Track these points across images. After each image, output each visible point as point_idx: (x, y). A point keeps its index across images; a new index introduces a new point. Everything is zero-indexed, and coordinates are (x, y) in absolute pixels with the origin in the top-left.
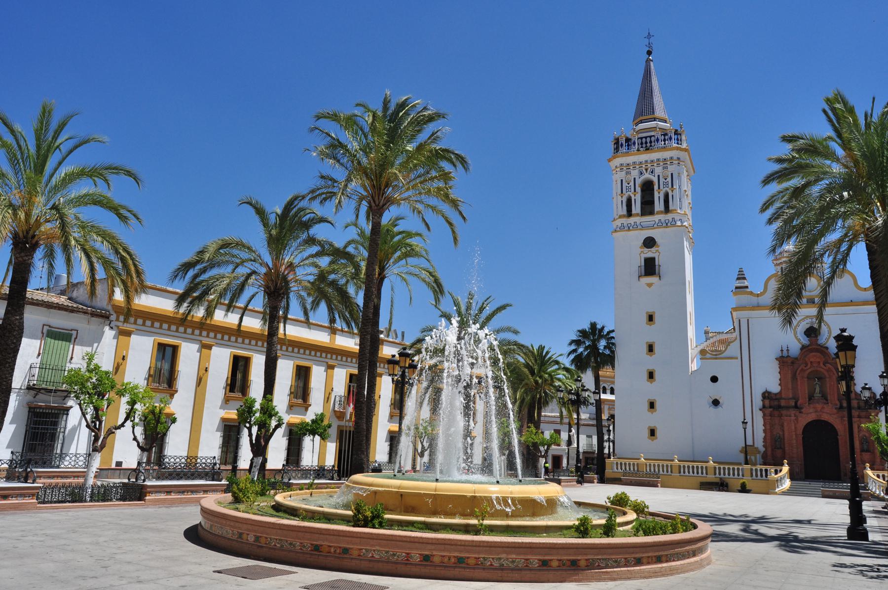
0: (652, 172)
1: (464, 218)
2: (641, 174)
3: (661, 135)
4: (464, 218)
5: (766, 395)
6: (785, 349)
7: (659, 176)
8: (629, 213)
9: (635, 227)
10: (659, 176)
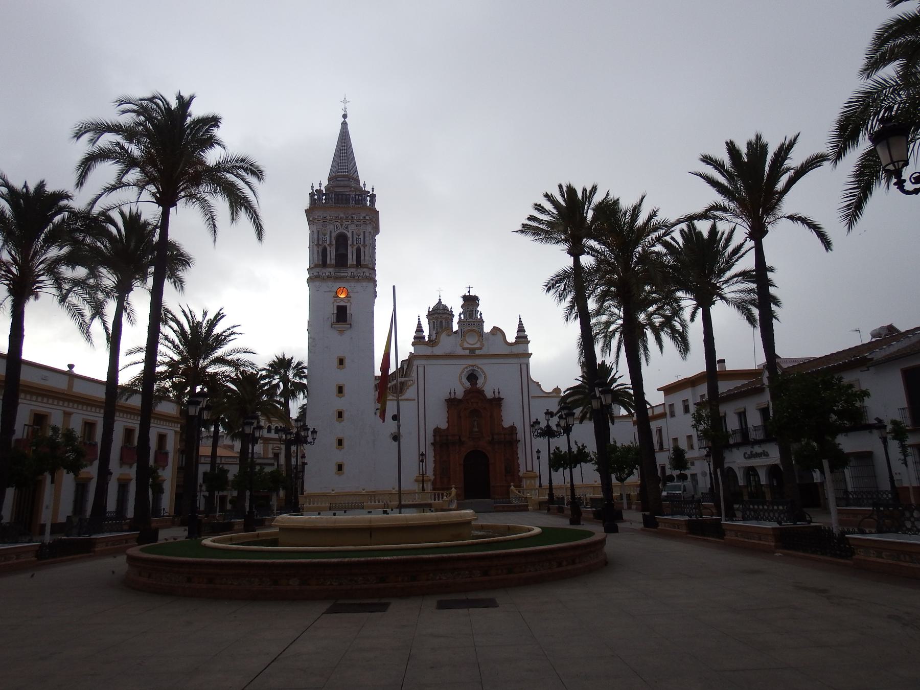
0: (347, 228)
2: (337, 228)
6: (452, 392)
7: (353, 232)
10: (353, 232)
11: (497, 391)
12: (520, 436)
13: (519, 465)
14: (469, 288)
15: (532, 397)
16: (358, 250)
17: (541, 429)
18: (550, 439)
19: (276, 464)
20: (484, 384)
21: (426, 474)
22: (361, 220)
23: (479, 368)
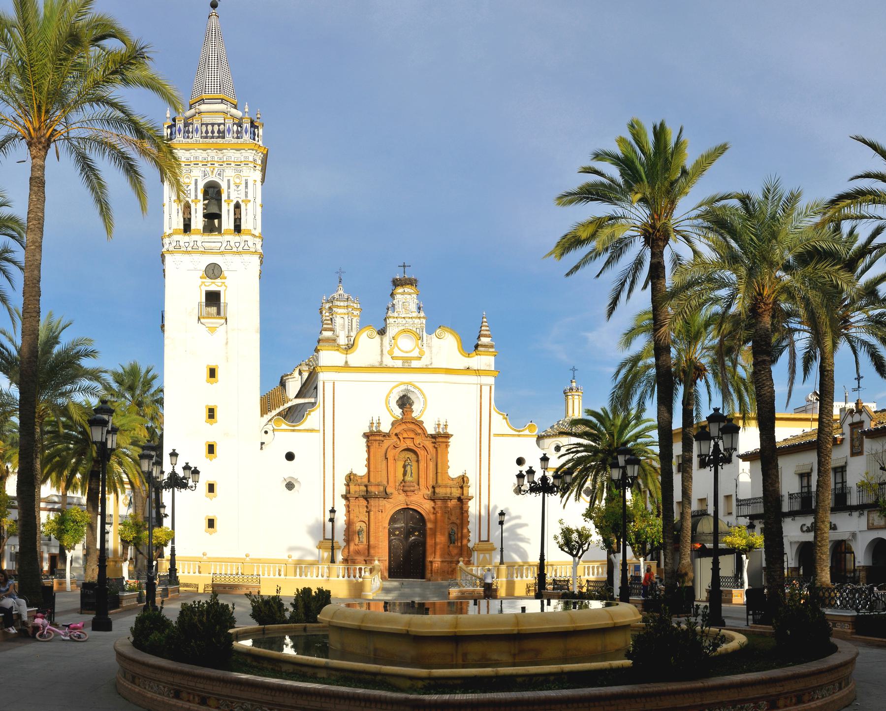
3: (234, 124)
5: (350, 478)
6: (442, 423)
7: (229, 181)
8: (187, 228)
9: (193, 250)
10: (229, 181)
12: (472, 491)
14: (404, 266)
16: (237, 206)
18: (546, 495)
20: (422, 412)
22: (191, 162)
23: (415, 387)
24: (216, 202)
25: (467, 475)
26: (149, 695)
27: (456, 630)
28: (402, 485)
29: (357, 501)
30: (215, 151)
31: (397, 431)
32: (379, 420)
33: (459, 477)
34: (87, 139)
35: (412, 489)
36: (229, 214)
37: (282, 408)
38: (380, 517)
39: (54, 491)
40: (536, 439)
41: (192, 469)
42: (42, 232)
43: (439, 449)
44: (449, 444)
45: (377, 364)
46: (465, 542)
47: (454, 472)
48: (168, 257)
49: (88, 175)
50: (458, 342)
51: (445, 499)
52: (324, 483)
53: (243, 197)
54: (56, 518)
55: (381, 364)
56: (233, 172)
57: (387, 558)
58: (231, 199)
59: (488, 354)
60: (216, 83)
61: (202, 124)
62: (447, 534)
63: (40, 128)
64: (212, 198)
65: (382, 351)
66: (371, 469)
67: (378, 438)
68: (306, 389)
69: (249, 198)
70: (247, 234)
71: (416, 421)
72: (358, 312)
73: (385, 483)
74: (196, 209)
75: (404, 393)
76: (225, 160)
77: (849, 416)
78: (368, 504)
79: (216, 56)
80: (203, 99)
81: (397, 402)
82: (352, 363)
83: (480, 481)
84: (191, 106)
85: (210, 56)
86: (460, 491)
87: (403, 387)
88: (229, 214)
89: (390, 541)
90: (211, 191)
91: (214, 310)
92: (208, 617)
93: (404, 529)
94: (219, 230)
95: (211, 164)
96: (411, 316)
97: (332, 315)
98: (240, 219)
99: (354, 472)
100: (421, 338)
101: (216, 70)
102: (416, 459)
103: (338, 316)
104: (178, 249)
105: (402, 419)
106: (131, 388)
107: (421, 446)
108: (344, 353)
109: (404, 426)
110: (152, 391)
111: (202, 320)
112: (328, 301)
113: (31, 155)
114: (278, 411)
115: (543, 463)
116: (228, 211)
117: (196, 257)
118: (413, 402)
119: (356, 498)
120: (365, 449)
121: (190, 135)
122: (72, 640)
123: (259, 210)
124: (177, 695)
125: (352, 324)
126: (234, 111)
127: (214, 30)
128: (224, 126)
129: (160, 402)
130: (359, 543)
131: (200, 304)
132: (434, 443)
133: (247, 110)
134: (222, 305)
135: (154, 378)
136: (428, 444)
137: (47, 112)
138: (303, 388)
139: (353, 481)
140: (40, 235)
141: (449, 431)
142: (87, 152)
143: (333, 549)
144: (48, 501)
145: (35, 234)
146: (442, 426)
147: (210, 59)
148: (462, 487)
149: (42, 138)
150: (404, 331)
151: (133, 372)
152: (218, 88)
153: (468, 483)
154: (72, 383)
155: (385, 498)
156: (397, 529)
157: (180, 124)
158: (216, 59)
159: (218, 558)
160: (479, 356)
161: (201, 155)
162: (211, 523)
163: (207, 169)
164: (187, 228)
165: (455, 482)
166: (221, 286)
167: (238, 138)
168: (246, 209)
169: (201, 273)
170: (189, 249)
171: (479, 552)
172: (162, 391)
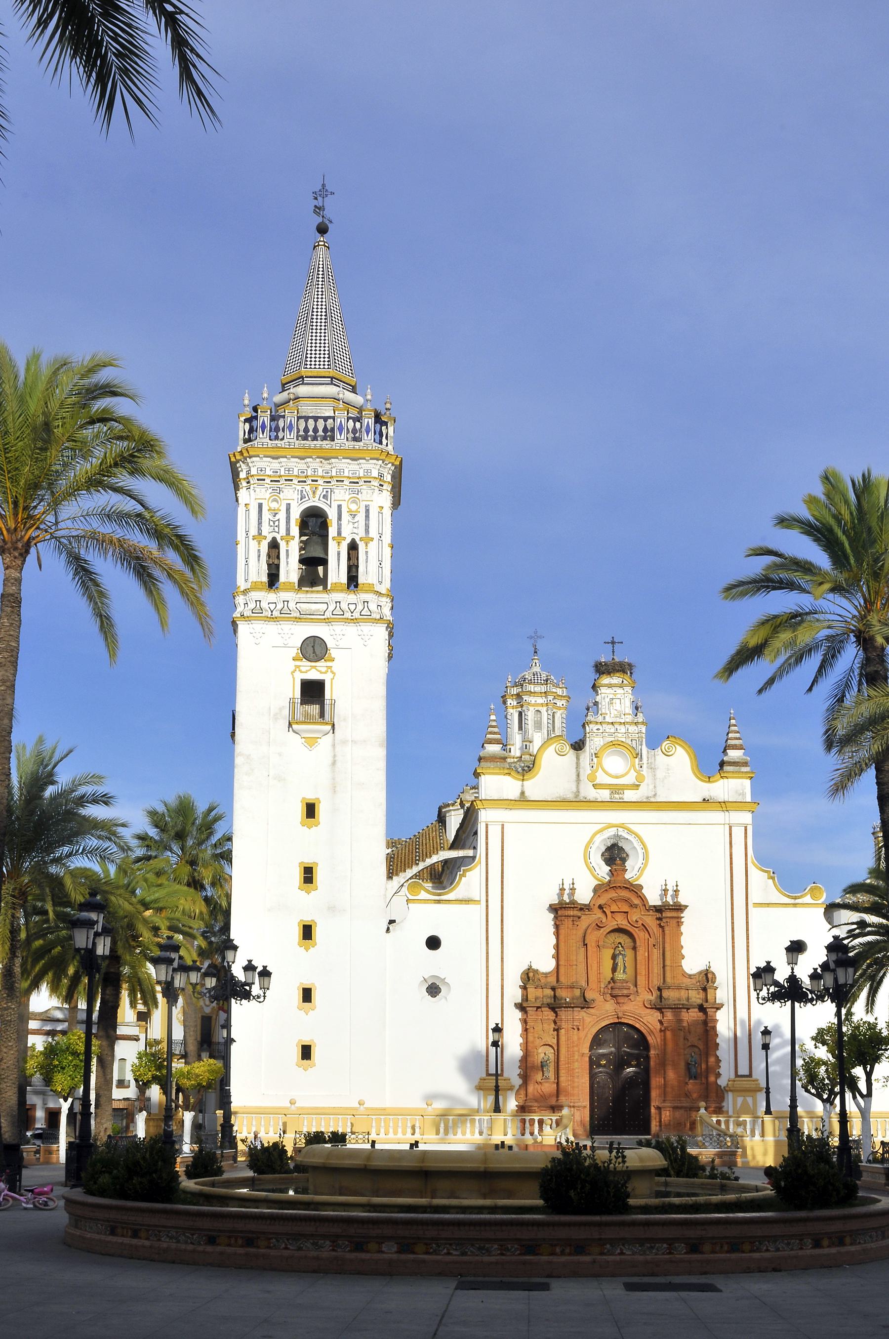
1: (810, 689)
3: (349, 418)
4: (810, 689)
5: (529, 977)
6: (670, 888)
7: (340, 507)
8: (273, 579)
10: (340, 507)
11: (670, 888)
12: (722, 994)
13: (718, 1061)
14: (613, 643)
15: (757, 905)
16: (353, 547)
17: (776, 983)
19: (142, 1037)
20: (641, 870)
21: (502, 1075)
22: (280, 476)
23: (630, 832)
24: (319, 540)
25: (711, 969)
26: (89, 1235)
27: (422, 1165)
28: (609, 987)
29: (539, 1013)
30: (318, 460)
31: (601, 901)
32: (573, 884)
33: (700, 973)
34: (81, 537)
35: (625, 992)
36: (339, 560)
37: (422, 865)
38: (575, 1038)
39: (55, 1002)
40: (823, 910)
41: (258, 970)
42: (16, 667)
43: (666, 929)
44: (683, 920)
45: (570, 796)
46: (712, 1079)
47: (692, 965)
48: (242, 627)
49: (84, 581)
50: (691, 759)
51: (677, 1009)
52: (487, 985)
53: (362, 533)
54: (45, 1048)
55: (577, 796)
56: (347, 492)
57: (587, 1103)
58: (342, 535)
59: (739, 775)
60: (322, 352)
61: (299, 418)
62: (682, 1065)
63: (16, 529)
64: (314, 533)
65: (578, 775)
66: (562, 963)
67: (571, 913)
68: (464, 832)
69: (371, 535)
70: (367, 591)
71: (632, 885)
72: (564, 702)
73: (583, 983)
74: (287, 551)
75: (612, 842)
76: (334, 474)
77: (221, 1012)
78: (556, 1017)
79: (324, 310)
80: (302, 377)
81: (602, 855)
82: (531, 795)
83: (734, 978)
84: (283, 385)
85: (315, 310)
86: (702, 995)
87: (612, 832)
88: (339, 560)
89: (592, 1076)
90: (312, 522)
91: (314, 709)
92: (151, 1154)
93: (615, 1057)
94: (324, 582)
95: (313, 481)
96: (622, 721)
97: (522, 706)
98: (357, 567)
99: (534, 967)
100: (638, 755)
101: (323, 331)
102: (632, 944)
103: (531, 708)
104: (258, 614)
105: (610, 881)
106: (180, 836)
107: (639, 924)
108: (518, 779)
109: (613, 894)
110: (214, 839)
111: (295, 726)
112: (516, 685)
113: (4, 564)
114: (415, 870)
115: (790, 955)
116: (339, 554)
117: (287, 627)
118: (627, 855)
119: (538, 1008)
120: (553, 930)
121: (281, 435)
122: (36, 1208)
123: (387, 552)
124: (113, 1232)
125: (554, 721)
126: (350, 396)
127: (321, 269)
128: (334, 421)
129: (227, 857)
130: (543, 1085)
131: (292, 701)
132: (659, 919)
133: (369, 397)
134: (327, 702)
135: (217, 819)
136: (650, 921)
137: (26, 508)
138: (461, 832)
139: (533, 981)
140: (12, 672)
141: (682, 900)
142: (82, 552)
143: (497, 1089)
144: (46, 1018)
145: (6, 671)
146: (670, 893)
147: (315, 314)
148: (705, 989)
149: (19, 543)
150: (613, 744)
151: (184, 809)
152: (326, 360)
153: (714, 983)
154: (71, 843)
155: (582, 1008)
156: (603, 1056)
157: (264, 418)
158: (324, 314)
159: (317, 1108)
160: (726, 780)
161: (296, 466)
162: (306, 1052)
163: (306, 487)
164: (273, 579)
165: (694, 981)
166: (325, 673)
167: (355, 439)
168: (367, 552)
169: (294, 652)
170: (276, 614)
171: (735, 1093)
172: (230, 839)
